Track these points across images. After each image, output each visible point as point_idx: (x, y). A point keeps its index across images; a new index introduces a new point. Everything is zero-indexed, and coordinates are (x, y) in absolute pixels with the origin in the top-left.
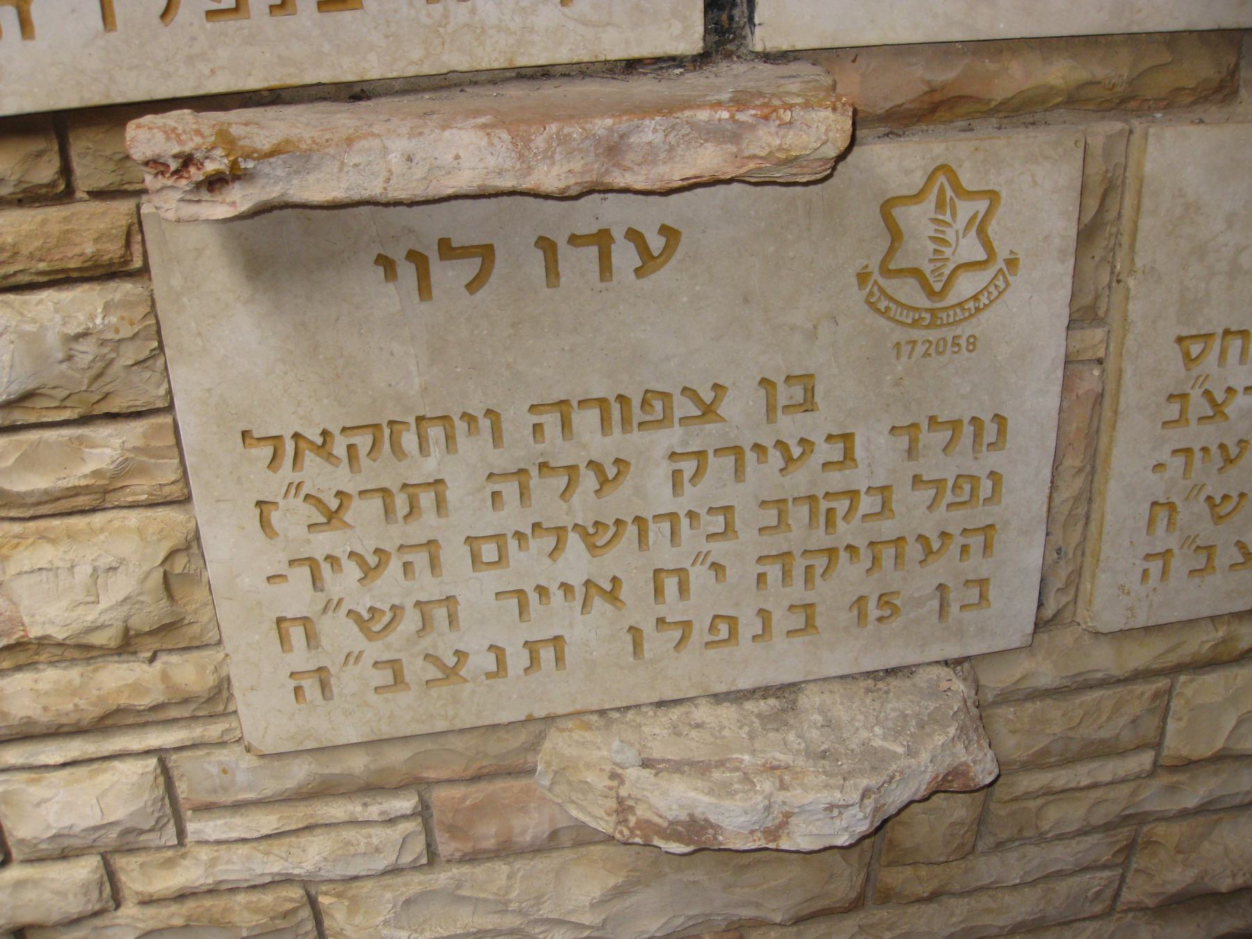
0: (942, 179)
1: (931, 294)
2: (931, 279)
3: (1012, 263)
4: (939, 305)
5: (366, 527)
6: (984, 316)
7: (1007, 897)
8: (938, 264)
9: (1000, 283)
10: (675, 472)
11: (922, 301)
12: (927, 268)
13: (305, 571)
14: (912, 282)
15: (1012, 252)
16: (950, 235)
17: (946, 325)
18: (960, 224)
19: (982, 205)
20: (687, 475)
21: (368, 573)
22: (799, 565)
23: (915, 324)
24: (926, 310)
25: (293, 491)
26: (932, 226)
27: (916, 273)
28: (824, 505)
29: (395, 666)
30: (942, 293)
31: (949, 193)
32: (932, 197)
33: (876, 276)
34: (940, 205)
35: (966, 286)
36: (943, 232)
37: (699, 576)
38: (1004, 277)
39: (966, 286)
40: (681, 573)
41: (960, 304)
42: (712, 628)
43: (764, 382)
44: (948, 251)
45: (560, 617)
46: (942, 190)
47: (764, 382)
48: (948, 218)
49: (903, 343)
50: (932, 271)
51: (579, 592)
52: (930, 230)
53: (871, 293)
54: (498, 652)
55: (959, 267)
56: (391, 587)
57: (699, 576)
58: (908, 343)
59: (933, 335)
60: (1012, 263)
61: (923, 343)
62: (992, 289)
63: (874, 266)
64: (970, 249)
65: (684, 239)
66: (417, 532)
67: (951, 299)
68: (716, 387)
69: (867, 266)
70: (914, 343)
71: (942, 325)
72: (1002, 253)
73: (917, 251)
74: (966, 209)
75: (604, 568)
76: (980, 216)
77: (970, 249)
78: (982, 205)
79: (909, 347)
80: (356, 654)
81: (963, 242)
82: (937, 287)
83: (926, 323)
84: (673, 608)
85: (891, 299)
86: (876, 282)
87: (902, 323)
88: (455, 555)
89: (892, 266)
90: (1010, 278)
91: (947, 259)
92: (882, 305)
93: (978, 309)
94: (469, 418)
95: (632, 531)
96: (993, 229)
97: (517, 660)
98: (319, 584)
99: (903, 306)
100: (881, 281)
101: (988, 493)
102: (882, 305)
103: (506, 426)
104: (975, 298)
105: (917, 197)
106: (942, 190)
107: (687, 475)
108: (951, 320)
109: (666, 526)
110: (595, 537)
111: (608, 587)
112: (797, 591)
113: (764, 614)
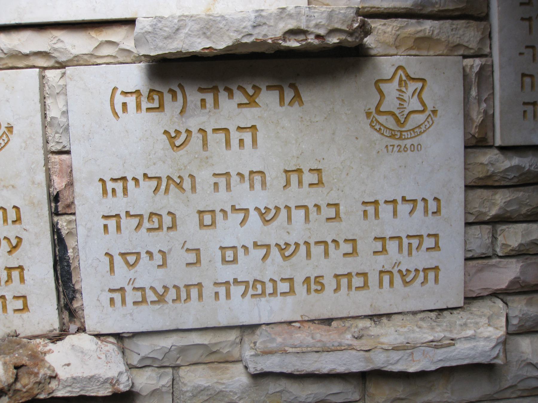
2: (399, 116)
3: (434, 112)
4: (403, 129)
6: (424, 135)
8: (402, 110)
9: (429, 119)
10: (409, 243)
12: (397, 112)
14: (391, 119)
15: (434, 107)
16: (406, 97)
17: (408, 138)
20: (415, 246)
26: (398, 93)
27: (392, 114)
28: (405, 241)
30: (402, 124)
31: (404, 78)
34: (400, 84)
36: (400, 95)
38: (432, 119)
41: (413, 130)
43: (101, 180)
44: (405, 105)
46: (401, 77)
47: (101, 180)
50: (399, 113)
52: (397, 94)
53: (372, 121)
58: (391, 145)
60: (434, 112)
61: (397, 146)
62: (426, 123)
63: (373, 110)
64: (414, 104)
69: (370, 109)
70: (393, 146)
71: (405, 139)
72: (430, 107)
74: (413, 86)
78: (419, 85)
79: (392, 147)
81: (411, 100)
83: (398, 136)
85: (382, 125)
86: (374, 117)
90: (434, 119)
91: (405, 108)
92: (377, 127)
94: (149, 253)
95: (284, 213)
96: (424, 96)
98: (156, 192)
103: (268, 179)
106: (401, 77)
107: (415, 246)
108: (409, 136)
111: (178, 181)
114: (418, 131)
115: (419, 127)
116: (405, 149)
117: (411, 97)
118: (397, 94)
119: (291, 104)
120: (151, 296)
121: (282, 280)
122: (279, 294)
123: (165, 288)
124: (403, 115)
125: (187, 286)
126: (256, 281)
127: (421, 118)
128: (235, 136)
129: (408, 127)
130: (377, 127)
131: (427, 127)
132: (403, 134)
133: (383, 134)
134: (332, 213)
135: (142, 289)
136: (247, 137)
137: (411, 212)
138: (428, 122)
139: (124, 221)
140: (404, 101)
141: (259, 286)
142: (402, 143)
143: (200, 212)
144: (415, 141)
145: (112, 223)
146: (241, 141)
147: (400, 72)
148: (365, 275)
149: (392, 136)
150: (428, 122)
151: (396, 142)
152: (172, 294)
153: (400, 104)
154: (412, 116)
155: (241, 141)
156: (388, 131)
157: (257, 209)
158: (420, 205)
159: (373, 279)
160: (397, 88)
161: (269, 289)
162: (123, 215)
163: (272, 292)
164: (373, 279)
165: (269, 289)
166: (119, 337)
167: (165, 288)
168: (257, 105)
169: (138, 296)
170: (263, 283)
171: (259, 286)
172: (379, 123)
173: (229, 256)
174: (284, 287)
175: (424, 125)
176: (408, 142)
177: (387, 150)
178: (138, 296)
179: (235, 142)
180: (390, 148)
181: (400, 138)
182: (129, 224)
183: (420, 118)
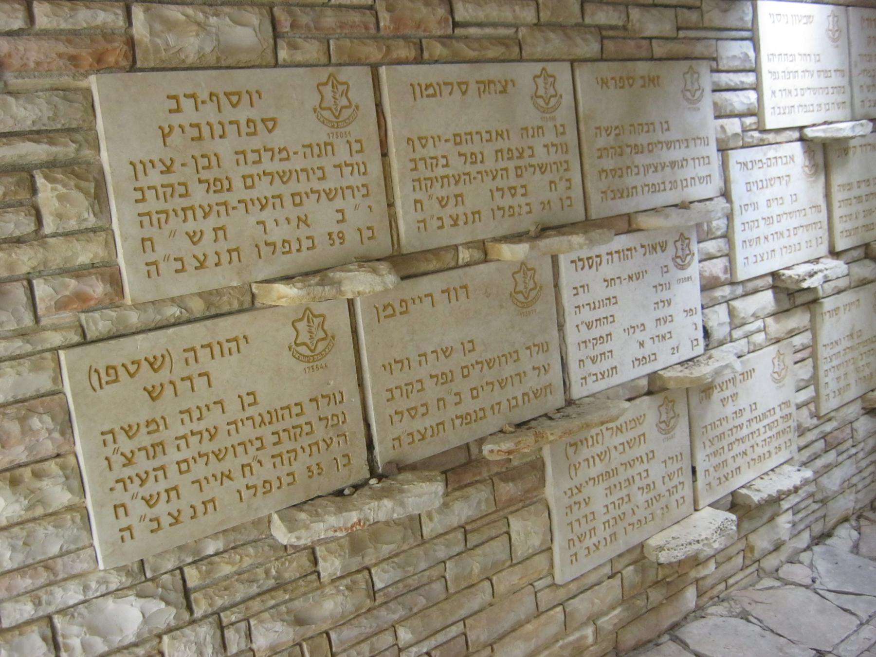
1: (312, 351)
3: (333, 337)
5: (143, 464)
6: (329, 355)
12: (308, 342)
13: (121, 484)
14: (304, 347)
18: (316, 326)
19: (321, 319)
21: (143, 482)
22: (285, 457)
29: (157, 520)
33: (318, 109)
34: (308, 322)
35: (321, 347)
37: (255, 465)
40: (249, 465)
42: (264, 487)
44: (314, 336)
45: (213, 490)
51: (219, 476)
54: (465, 214)
56: (151, 488)
57: (255, 465)
63: (318, 107)
65: (469, 285)
66: (157, 463)
67: (317, 352)
68: (178, 511)
75: (224, 466)
78: (321, 319)
80: (437, 143)
82: (313, 348)
84: (251, 481)
88: (172, 470)
92: (322, 119)
96: (350, 95)
97: (200, 508)
101: (228, 187)
102: (297, 356)
104: (324, 350)
110: (218, 456)
112: (287, 469)
113: (279, 478)
115: (348, 118)
127: (350, 111)
130: (297, 356)
141: (218, 183)
142: (339, 130)
143: (178, 463)
144: (322, 362)
149: (333, 127)
157: (213, 452)
171: (218, 183)
173: (184, 467)
176: (342, 130)
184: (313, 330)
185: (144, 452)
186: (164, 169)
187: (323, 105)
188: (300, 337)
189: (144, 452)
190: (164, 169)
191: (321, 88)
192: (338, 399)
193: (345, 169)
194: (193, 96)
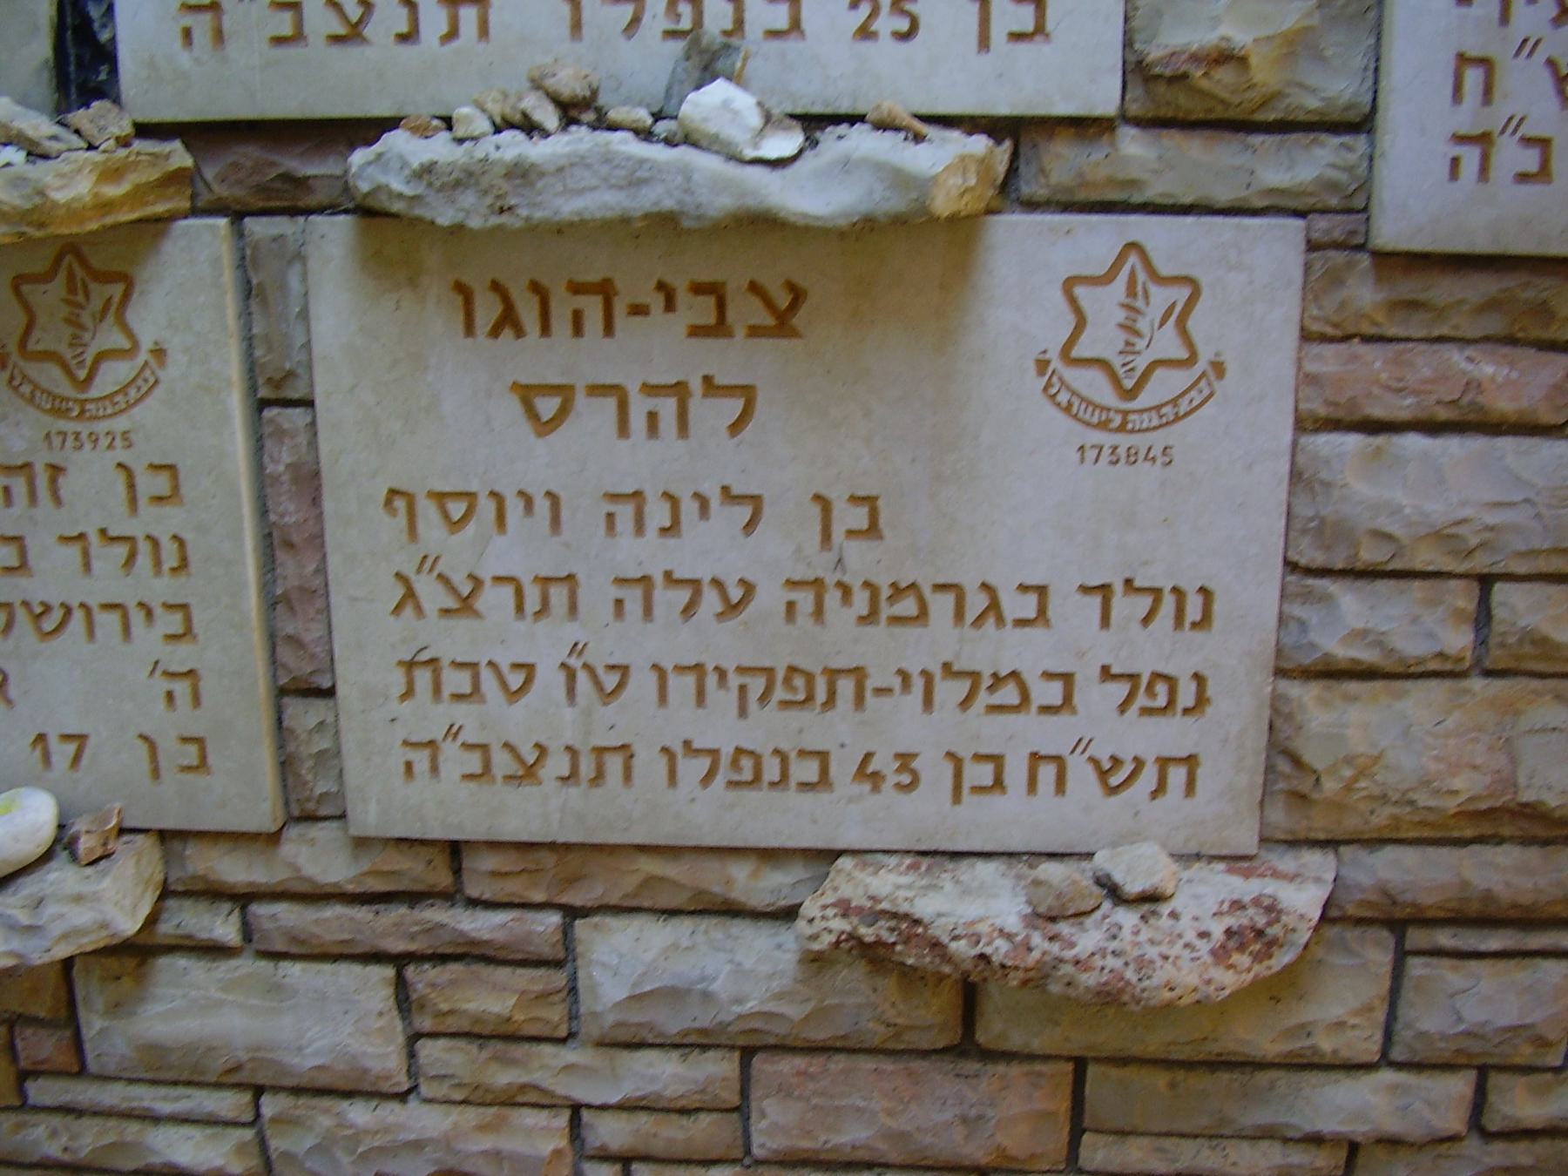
0: (1133, 259)
2: (1121, 372)
4: (84, 396)
7: (1206, 1152)
11: (65, 388)
12: (1117, 362)
23: (1103, 426)
24: (1118, 411)
25: (580, 646)
30: (1131, 394)
31: (1141, 276)
32: (62, 276)
33: (1056, 364)
34: (72, 289)
35: (1165, 385)
39: (1165, 385)
41: (1158, 408)
44: (1141, 344)
48: (80, 298)
49: (1088, 446)
50: (74, 357)
52: (1121, 315)
53: (12, 378)
55: (100, 357)
59: (1124, 441)
64: (1167, 344)
71: (1132, 431)
72: (1205, 355)
73: (1102, 340)
74: (1161, 297)
76: (1178, 309)
77: (1167, 344)
78: (1181, 294)
83: (75, 413)
87: (1088, 424)
89: (1075, 353)
91: (1138, 353)
92: (1063, 398)
93: (1178, 418)
96: (1194, 324)
99: (1089, 403)
100: (22, 363)
105: (1107, 279)
108: (1145, 425)
109: (690, 680)
114: (1173, 413)
116: (1132, 457)
117: (1156, 325)
118: (1121, 315)
119: (495, 332)
120: (502, 763)
121: (803, 753)
122: (765, 785)
123: (542, 750)
124: (1132, 369)
125: (600, 751)
126: (739, 751)
128: (639, 409)
129: (1145, 399)
131: (1195, 403)
132: (89, 406)
133: (1075, 416)
134: (174, 623)
135: (484, 748)
136: (667, 408)
137: (1146, 620)
138: (146, 380)
139: (661, 594)
140: (1138, 334)
144: (1158, 439)
145: (633, 598)
146: (652, 417)
147: (1133, 259)
148: (997, 760)
150: (146, 380)
151: (1106, 439)
152: (558, 764)
153: (1128, 343)
154: (1159, 373)
155: (652, 417)
156: (1090, 409)
158: (1168, 603)
159: (1016, 772)
160: (63, 294)
161: (772, 770)
162: (659, 579)
163: (776, 778)
164: (1016, 772)
165: (772, 770)
166: (165, 836)
167: (542, 750)
168: (793, 333)
169: (474, 763)
170: (756, 757)
172: (1068, 388)
174: (808, 771)
175: (1188, 397)
177: (50, 444)
178: (474, 763)
179: (638, 421)
180: (57, 441)
181: (1122, 429)
182: (670, 600)
183: (1175, 381)
184: (1143, 325)
185: (508, 592)
186: (451, 603)
187: (1081, 350)
188: (1084, 338)
189: (508, 592)
190: (451, 603)
191: (1080, 291)
192: (1193, 611)
193: (1120, 603)
194: (605, 290)
